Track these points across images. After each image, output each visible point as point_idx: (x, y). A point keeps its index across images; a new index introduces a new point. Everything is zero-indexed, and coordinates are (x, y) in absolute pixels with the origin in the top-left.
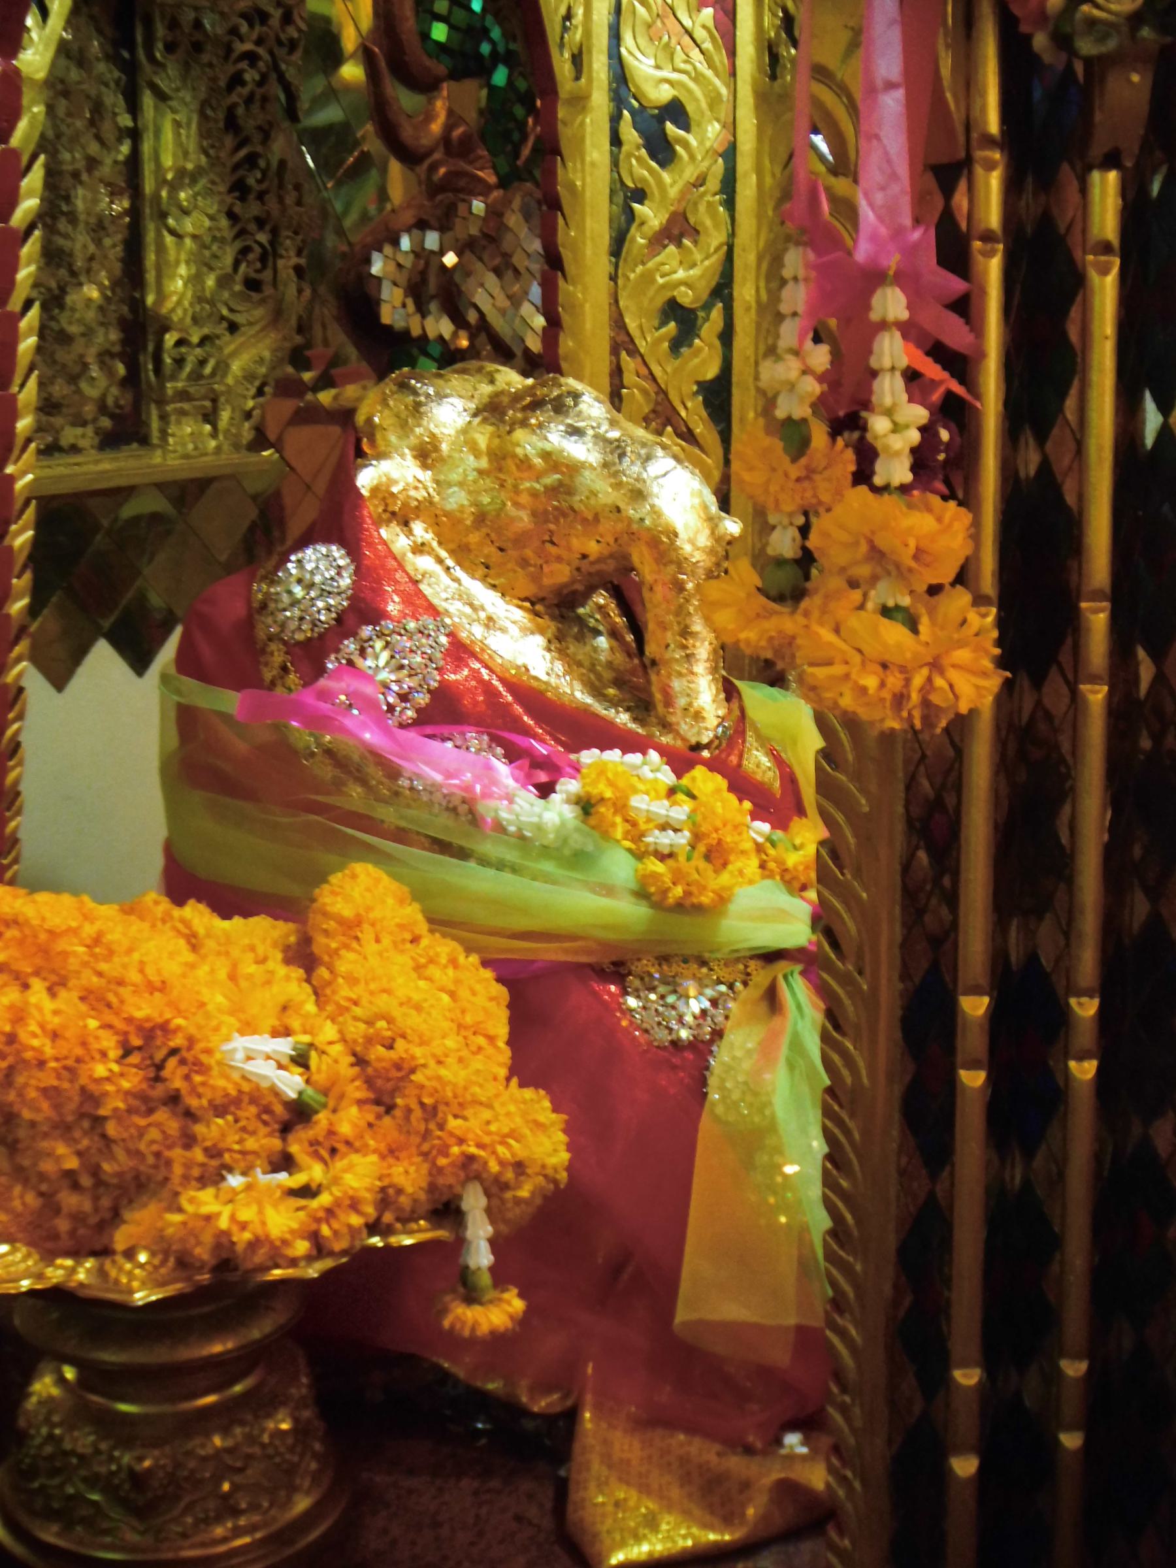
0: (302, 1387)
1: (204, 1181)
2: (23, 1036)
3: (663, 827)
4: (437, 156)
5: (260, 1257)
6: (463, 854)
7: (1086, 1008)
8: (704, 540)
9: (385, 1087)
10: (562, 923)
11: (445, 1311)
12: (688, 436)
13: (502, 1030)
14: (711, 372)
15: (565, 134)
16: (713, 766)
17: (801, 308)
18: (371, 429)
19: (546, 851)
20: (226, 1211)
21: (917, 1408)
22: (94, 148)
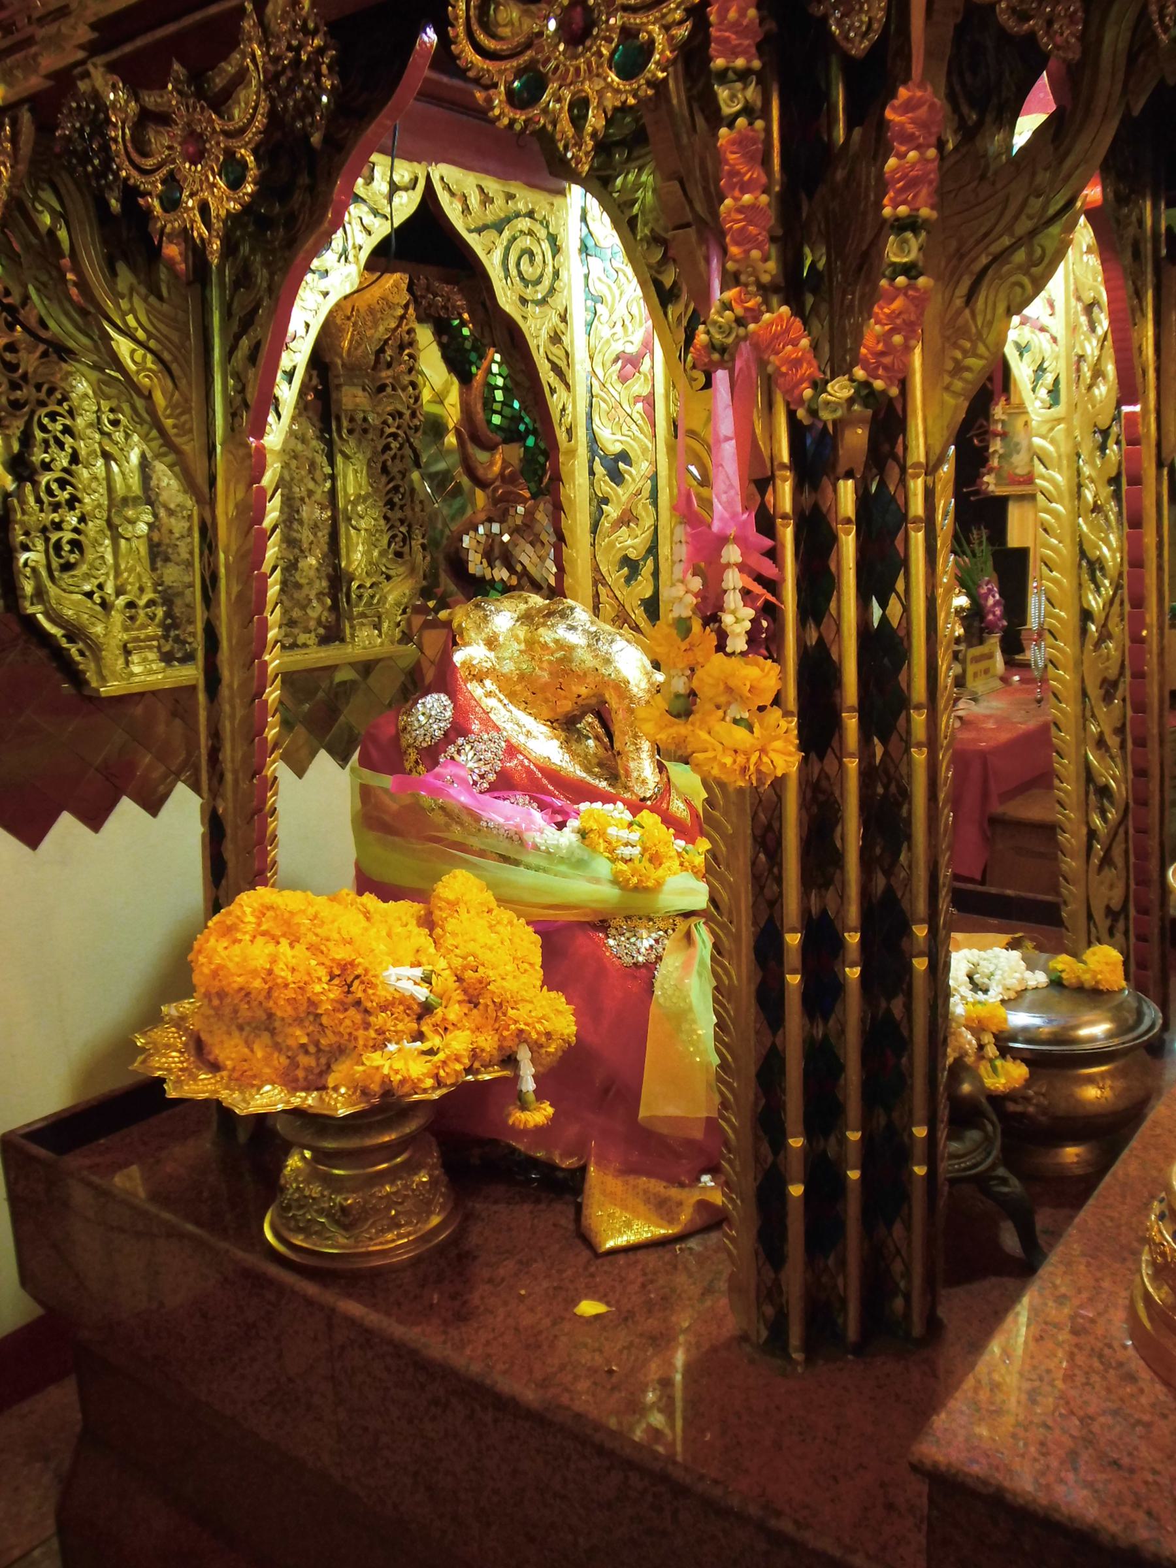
0: (434, 1158)
1: (375, 1048)
2: (277, 971)
3: (626, 845)
4: (497, 483)
5: (406, 1088)
6: (516, 863)
7: (853, 939)
8: (644, 685)
9: (473, 994)
10: (572, 899)
11: (509, 1115)
12: (636, 628)
13: (538, 960)
14: (648, 594)
15: (564, 470)
16: (652, 810)
17: (684, 557)
18: (461, 631)
19: (562, 860)
20: (387, 1064)
21: (770, 1159)
22: (311, 485)
